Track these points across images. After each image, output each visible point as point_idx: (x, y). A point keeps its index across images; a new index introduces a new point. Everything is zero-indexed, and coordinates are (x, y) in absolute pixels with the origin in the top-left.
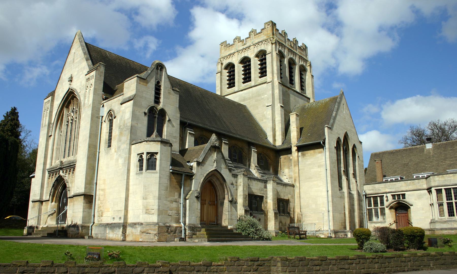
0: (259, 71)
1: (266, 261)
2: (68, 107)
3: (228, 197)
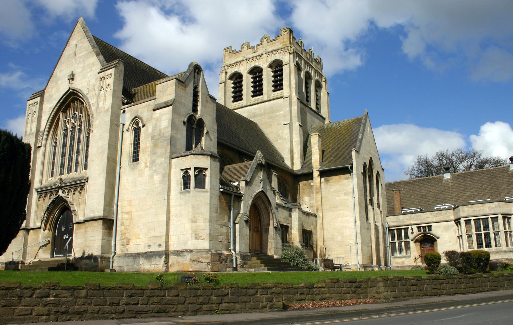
0: (273, 84)
1: (363, 282)
2: (65, 112)
3: (274, 223)
